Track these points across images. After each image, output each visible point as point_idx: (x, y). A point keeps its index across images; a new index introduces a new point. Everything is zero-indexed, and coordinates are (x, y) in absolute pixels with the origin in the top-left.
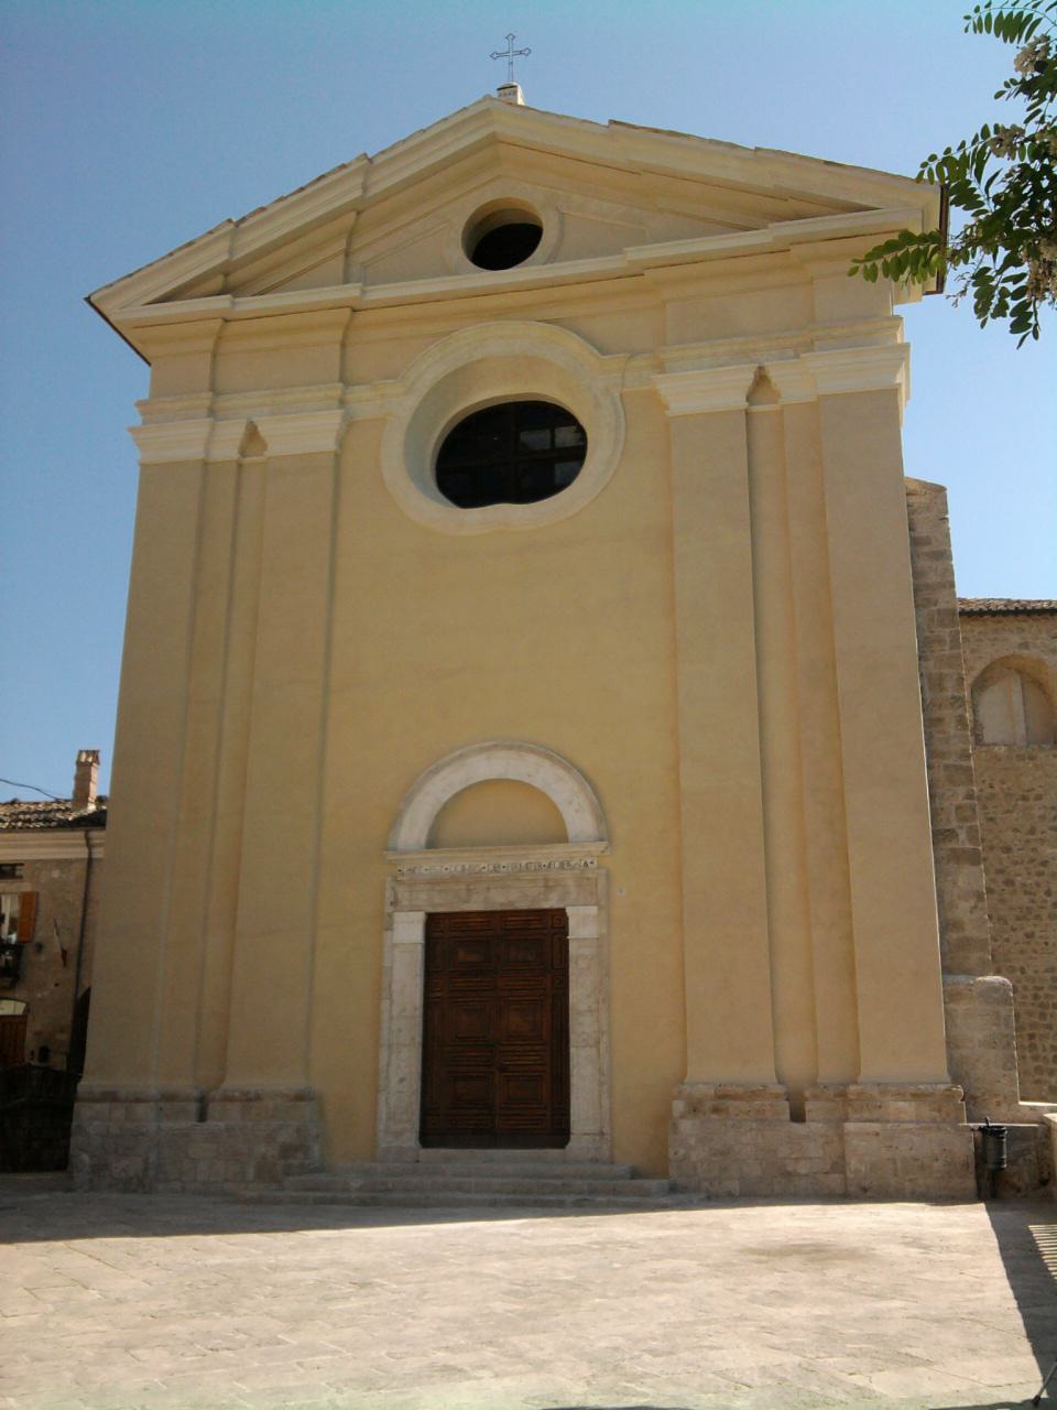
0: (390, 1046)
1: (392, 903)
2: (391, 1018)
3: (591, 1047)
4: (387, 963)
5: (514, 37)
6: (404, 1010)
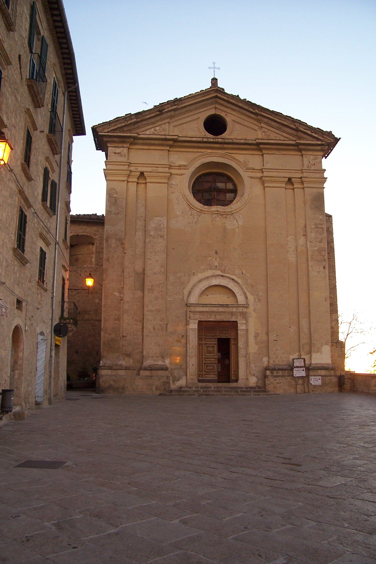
0: (190, 356)
1: (189, 318)
3: (244, 357)
4: (188, 334)
5: (215, 63)
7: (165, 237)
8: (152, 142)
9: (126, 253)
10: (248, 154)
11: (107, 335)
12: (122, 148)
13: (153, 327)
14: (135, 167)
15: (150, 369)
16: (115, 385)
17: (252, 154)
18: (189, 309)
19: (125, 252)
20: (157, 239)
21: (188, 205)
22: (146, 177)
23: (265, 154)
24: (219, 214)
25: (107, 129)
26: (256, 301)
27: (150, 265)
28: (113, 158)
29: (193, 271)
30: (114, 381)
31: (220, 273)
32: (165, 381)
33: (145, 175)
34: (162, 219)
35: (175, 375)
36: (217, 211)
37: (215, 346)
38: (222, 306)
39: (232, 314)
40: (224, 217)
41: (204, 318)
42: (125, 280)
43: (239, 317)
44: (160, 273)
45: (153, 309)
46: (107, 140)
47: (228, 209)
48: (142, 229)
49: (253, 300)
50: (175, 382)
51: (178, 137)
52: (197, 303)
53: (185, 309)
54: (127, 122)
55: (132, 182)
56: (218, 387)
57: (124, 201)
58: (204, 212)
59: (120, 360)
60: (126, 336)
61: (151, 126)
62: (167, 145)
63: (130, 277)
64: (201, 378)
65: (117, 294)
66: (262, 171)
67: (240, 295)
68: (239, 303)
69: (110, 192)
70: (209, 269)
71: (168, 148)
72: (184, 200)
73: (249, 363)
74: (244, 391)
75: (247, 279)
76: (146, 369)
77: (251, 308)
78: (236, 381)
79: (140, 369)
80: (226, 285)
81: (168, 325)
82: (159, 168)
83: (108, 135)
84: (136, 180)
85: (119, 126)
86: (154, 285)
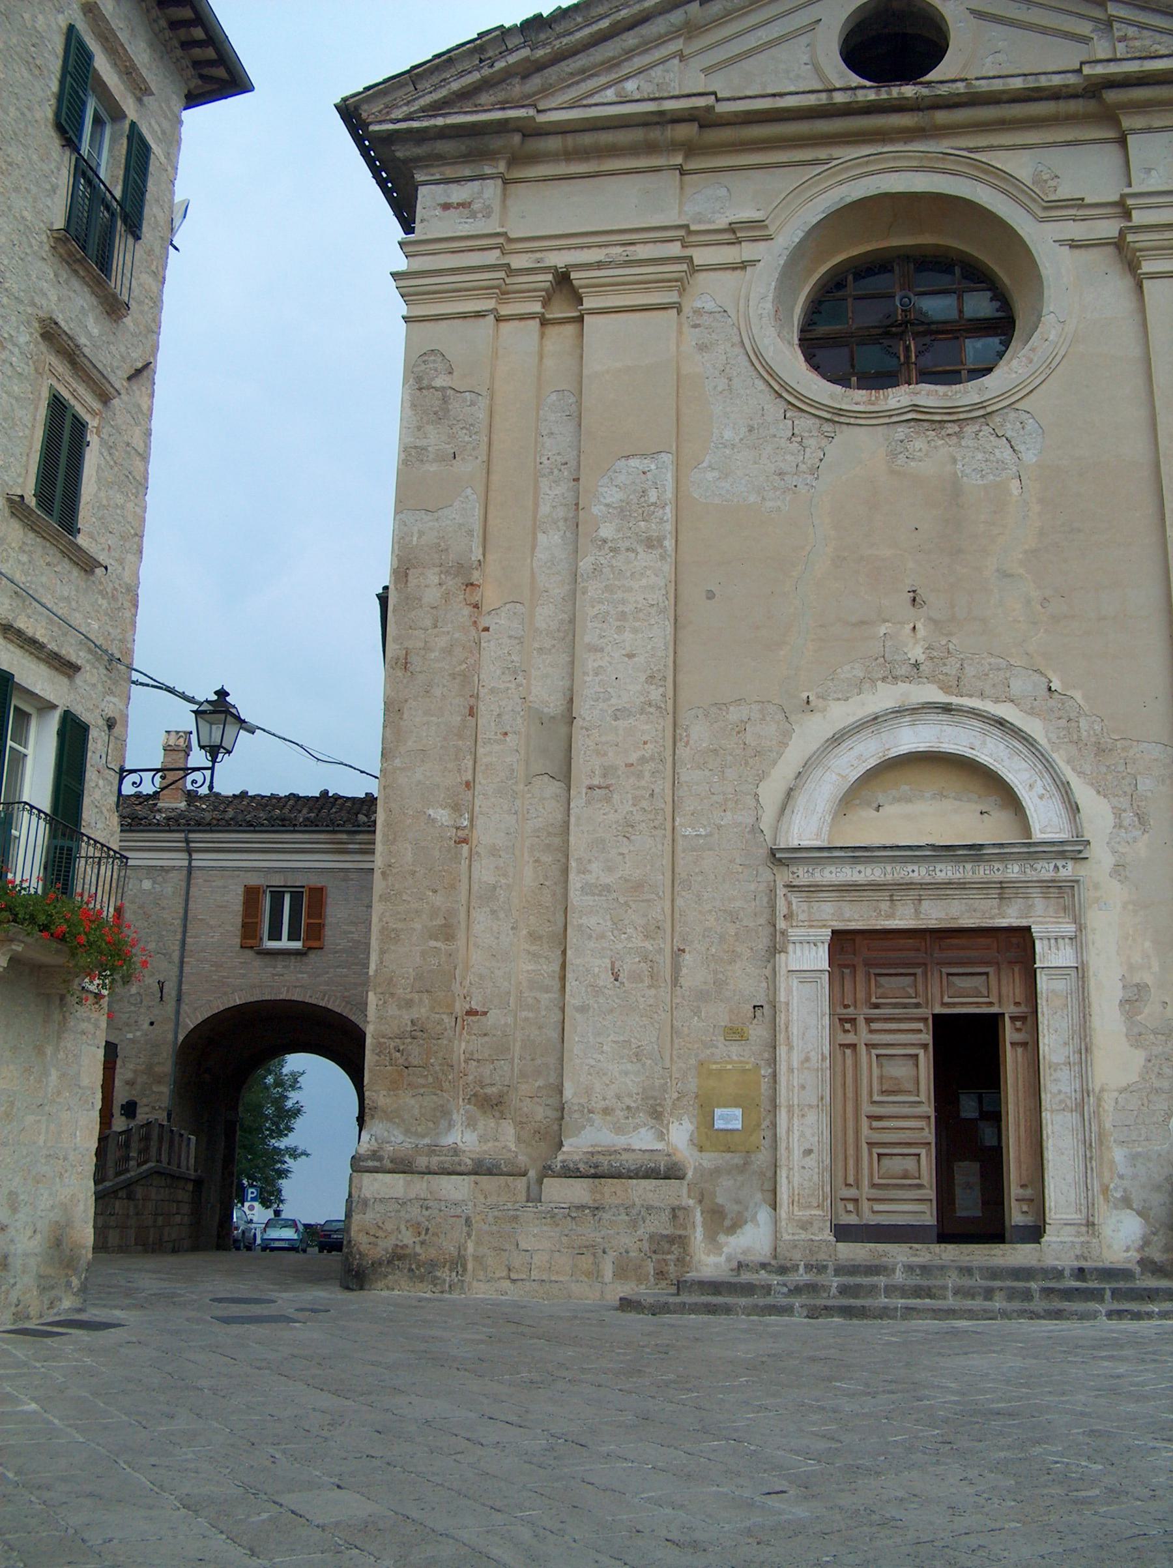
2: (791, 1070)
4: (782, 997)
6: (807, 1059)
7: (669, 544)
8: (606, 138)
9: (487, 629)
10: (1054, 144)
11: (392, 1010)
12: (477, 183)
13: (612, 969)
14: (530, 255)
15: (592, 1171)
16: (418, 1249)
17: (1068, 144)
18: (783, 876)
19: (484, 622)
20: (633, 555)
21: (773, 395)
22: (580, 291)
23: (1134, 131)
24: (925, 424)
25: (405, 104)
26: (1125, 823)
27: (597, 674)
28: (430, 223)
29: (804, 696)
30: (418, 1228)
31: (933, 694)
32: (665, 1232)
33: (574, 282)
34: (653, 467)
35: (720, 1200)
36: (915, 408)
37: (921, 1052)
38: (946, 852)
39: (1003, 890)
40: (950, 431)
41: (859, 917)
42: (481, 751)
43: (1039, 904)
44: (642, 711)
45: (607, 879)
46: (408, 154)
47: (967, 394)
48: (566, 520)
49: (1110, 819)
50: (722, 1238)
51: (717, 100)
52: (826, 844)
53: (771, 878)
54: (492, 66)
55: (522, 317)
56: (925, 1270)
57: (483, 402)
58: (852, 421)
59: (450, 1126)
60: (485, 1013)
61: (603, 80)
62: (674, 146)
63: (506, 734)
64: (852, 1219)
65: (442, 815)
66: (1123, 209)
67: (1041, 797)
68: (1038, 835)
69: (419, 369)
70: (884, 679)
71: (678, 160)
72: (754, 373)
73: (1101, 1142)
74: (1068, 1294)
75: (1073, 715)
76: (570, 1173)
77: (1101, 856)
78: (1035, 1233)
79: (547, 1171)
80: (969, 753)
81: (687, 956)
82: (638, 246)
83: (410, 131)
84: (537, 307)
85: (455, 86)
86: (616, 769)
